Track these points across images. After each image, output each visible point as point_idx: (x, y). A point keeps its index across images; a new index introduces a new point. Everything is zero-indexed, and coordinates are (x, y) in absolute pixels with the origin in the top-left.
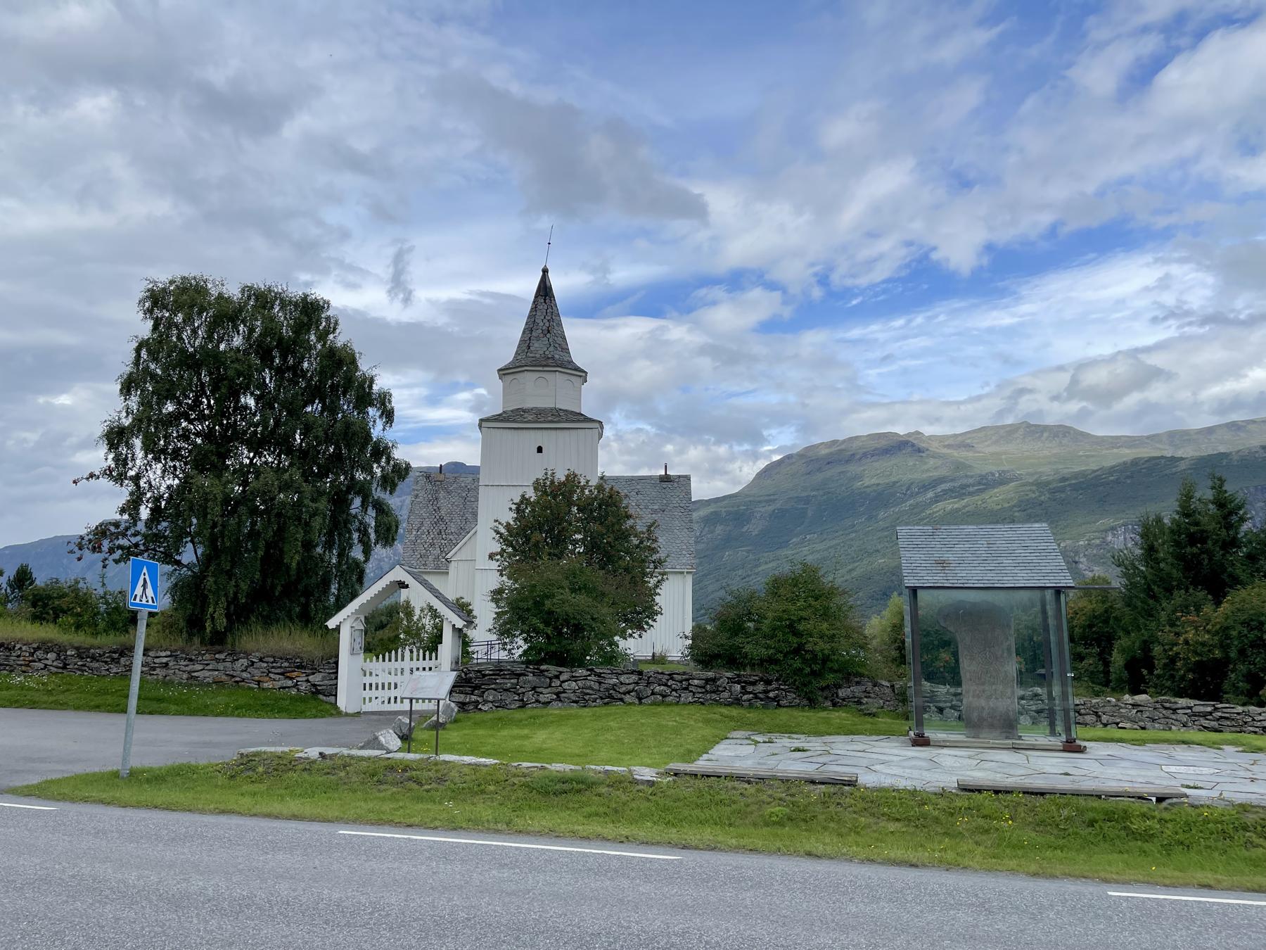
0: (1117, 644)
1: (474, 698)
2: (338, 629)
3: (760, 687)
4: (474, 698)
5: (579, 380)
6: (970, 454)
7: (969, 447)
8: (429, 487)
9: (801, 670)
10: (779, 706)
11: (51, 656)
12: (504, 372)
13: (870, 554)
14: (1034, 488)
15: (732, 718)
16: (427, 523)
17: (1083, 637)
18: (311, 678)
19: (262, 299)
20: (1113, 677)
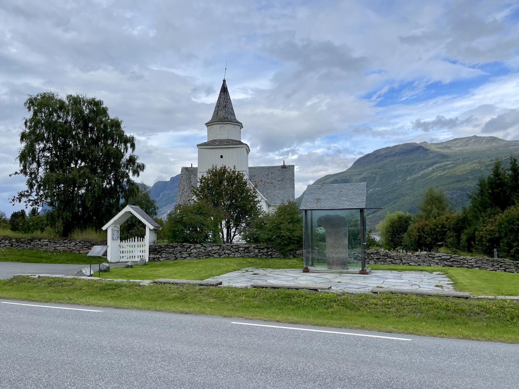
1: (158, 256)
2: (106, 230)
3: (265, 250)
4: (158, 256)
5: (238, 128)
6: (449, 151)
7: (449, 148)
8: (187, 173)
9: (280, 243)
10: (272, 257)
11: (7, 242)
12: (208, 124)
14: (478, 165)
15: (250, 262)
16: (186, 187)
17: (454, 229)
19: (76, 101)
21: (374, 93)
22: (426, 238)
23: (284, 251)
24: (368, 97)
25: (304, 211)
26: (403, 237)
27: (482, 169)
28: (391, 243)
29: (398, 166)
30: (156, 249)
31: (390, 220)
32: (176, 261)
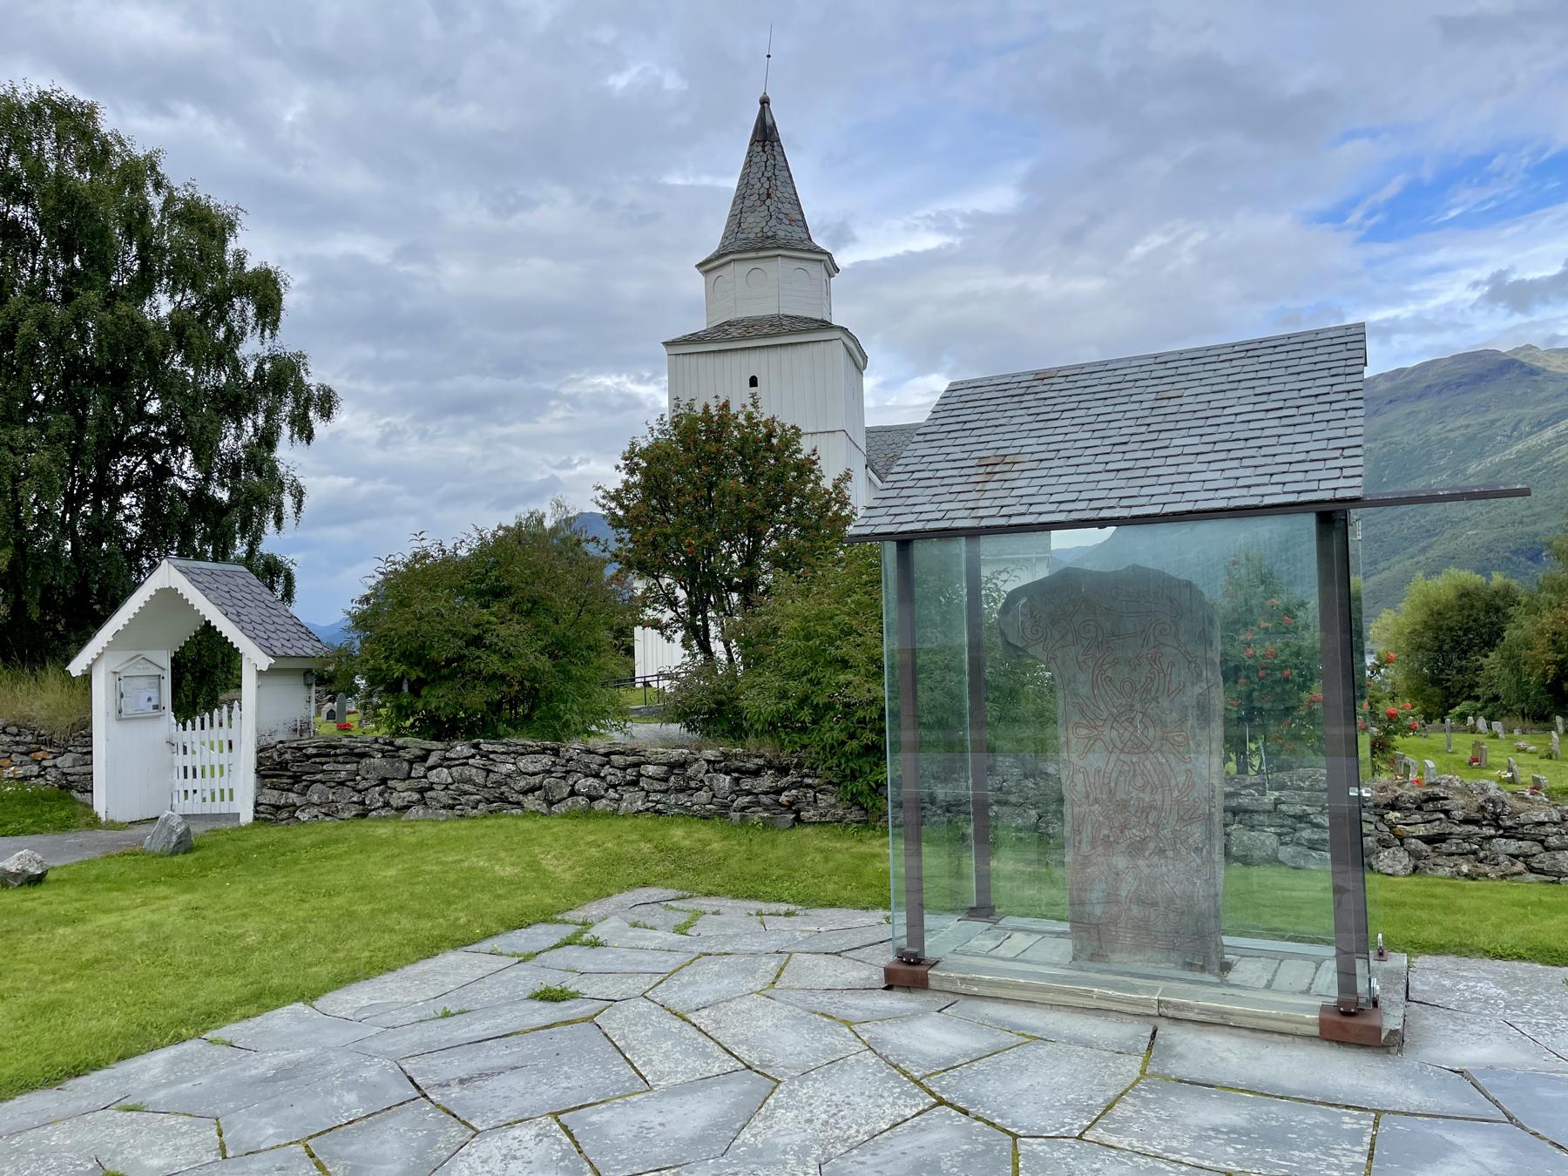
2: (87, 678)
3: (766, 781)
5: (818, 271)
12: (705, 267)
18: (59, 761)
21: (1354, 203)
23: (861, 785)
24: (1335, 216)
25: (891, 548)
26: (1481, 668)
28: (1430, 690)
29: (1435, 428)
30: (283, 765)
32: (364, 827)
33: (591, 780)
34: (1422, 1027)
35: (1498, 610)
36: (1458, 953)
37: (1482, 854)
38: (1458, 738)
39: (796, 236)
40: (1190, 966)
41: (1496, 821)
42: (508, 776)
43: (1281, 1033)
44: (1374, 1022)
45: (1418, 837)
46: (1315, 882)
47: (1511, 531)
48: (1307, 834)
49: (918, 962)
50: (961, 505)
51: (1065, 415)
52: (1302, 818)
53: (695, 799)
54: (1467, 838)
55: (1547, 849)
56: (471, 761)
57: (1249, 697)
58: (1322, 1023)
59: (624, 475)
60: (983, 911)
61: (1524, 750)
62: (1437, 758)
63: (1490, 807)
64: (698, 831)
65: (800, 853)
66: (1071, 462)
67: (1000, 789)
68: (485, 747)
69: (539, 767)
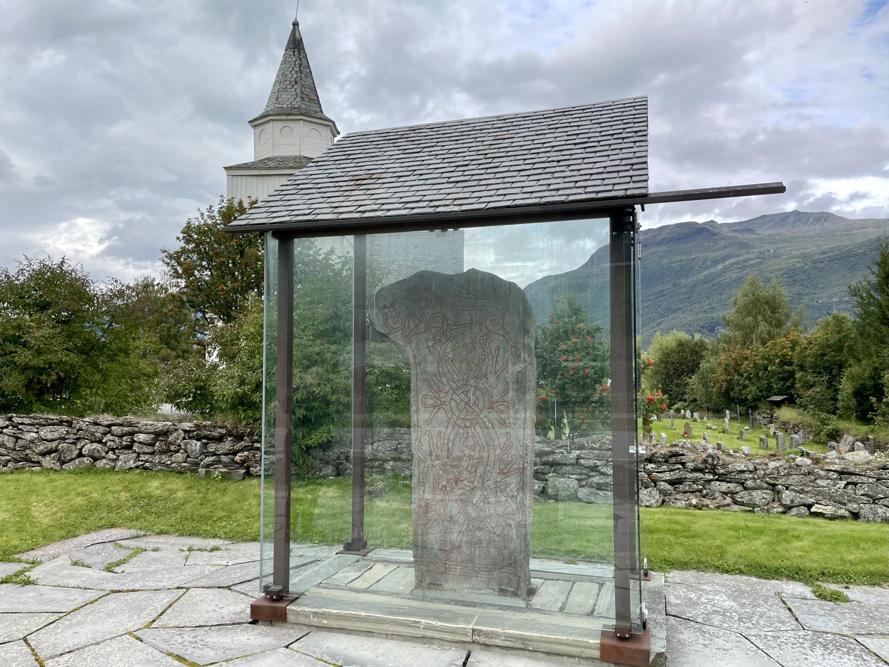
0: (847, 372)
3: (227, 445)
6: (752, 236)
7: (751, 231)
10: (248, 474)
12: (256, 123)
13: (674, 311)
14: (800, 260)
17: (814, 366)
20: (840, 404)
22: (745, 387)
27: (806, 267)
29: (665, 261)
31: (661, 349)
33: (95, 445)
34: (679, 641)
35: (697, 353)
36: (698, 569)
37: (704, 492)
38: (676, 421)
39: (313, 109)
40: (502, 592)
41: (713, 470)
42: (32, 441)
43: (570, 656)
44: (644, 646)
45: (665, 481)
46: (599, 515)
47: (700, 316)
48: (596, 479)
49: (280, 599)
50: (328, 205)
51: (425, 150)
52: (594, 468)
53: (173, 459)
54: (695, 481)
55: (745, 489)
56: (5, 430)
57: (562, 388)
58: (603, 647)
59: (182, 244)
60: (356, 545)
61: (710, 428)
62: (666, 432)
63: (710, 460)
64: (170, 483)
65: (243, 498)
66: (422, 177)
67: (396, 450)
68: (16, 420)
69: (56, 435)
